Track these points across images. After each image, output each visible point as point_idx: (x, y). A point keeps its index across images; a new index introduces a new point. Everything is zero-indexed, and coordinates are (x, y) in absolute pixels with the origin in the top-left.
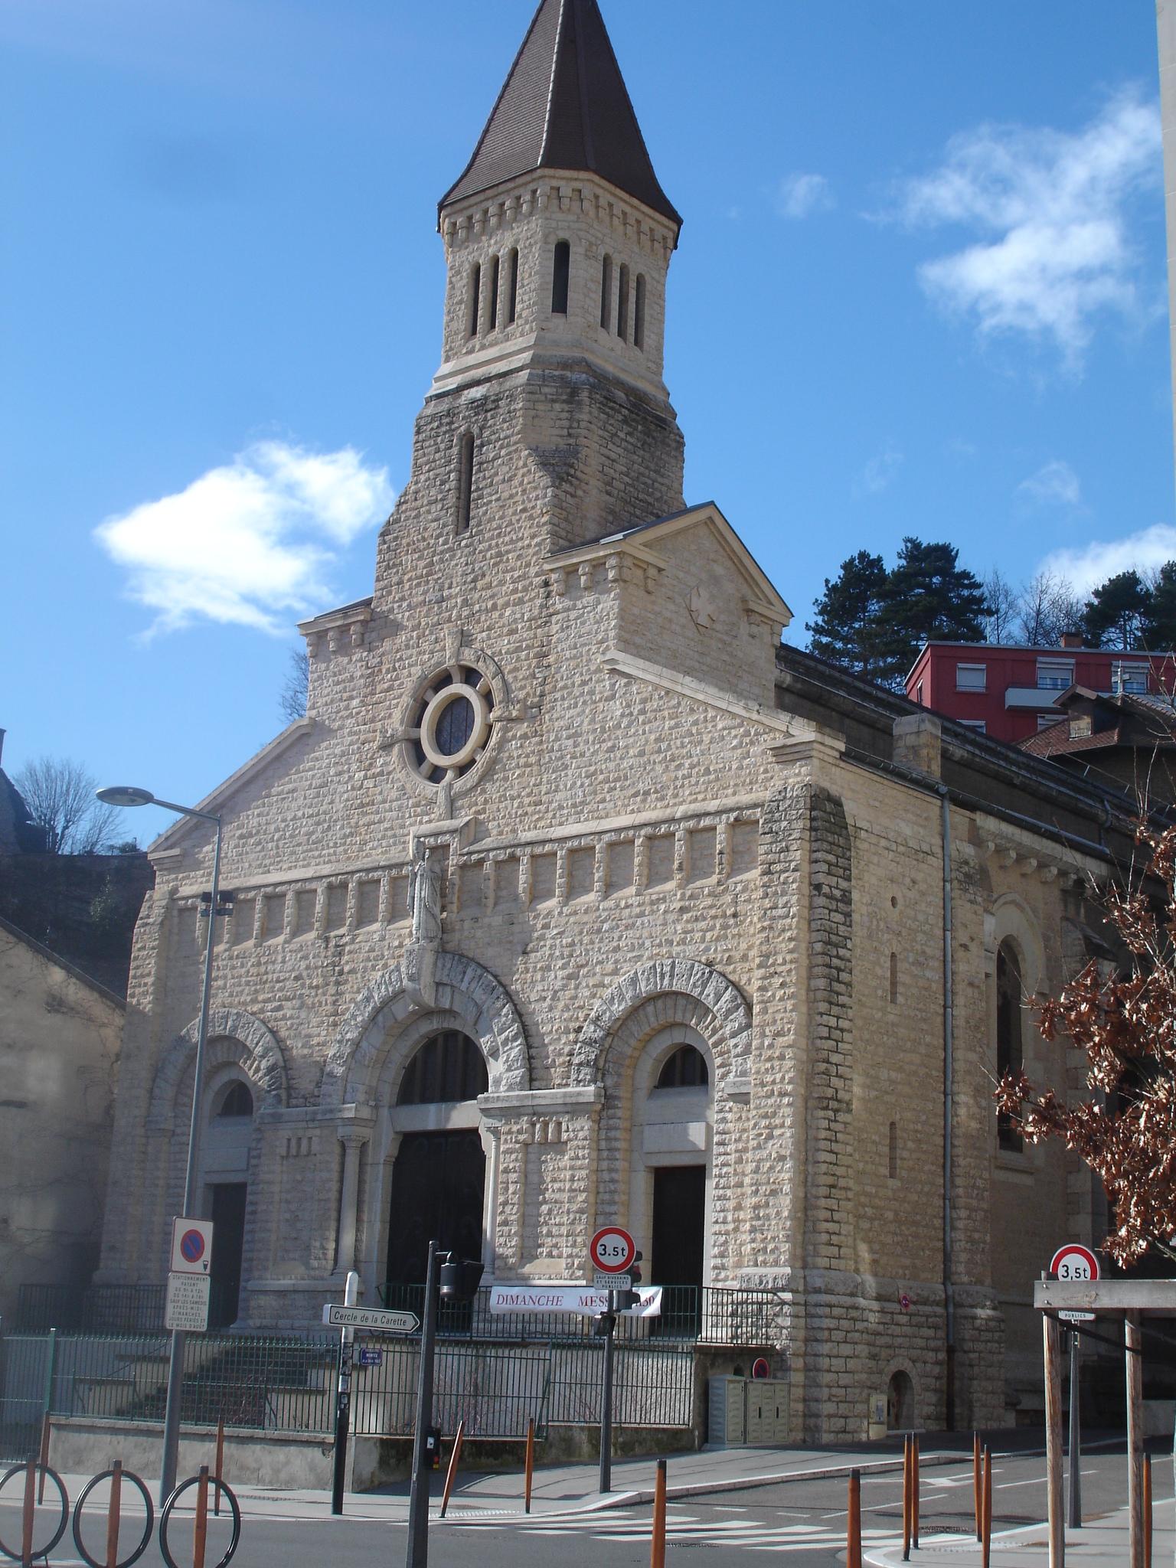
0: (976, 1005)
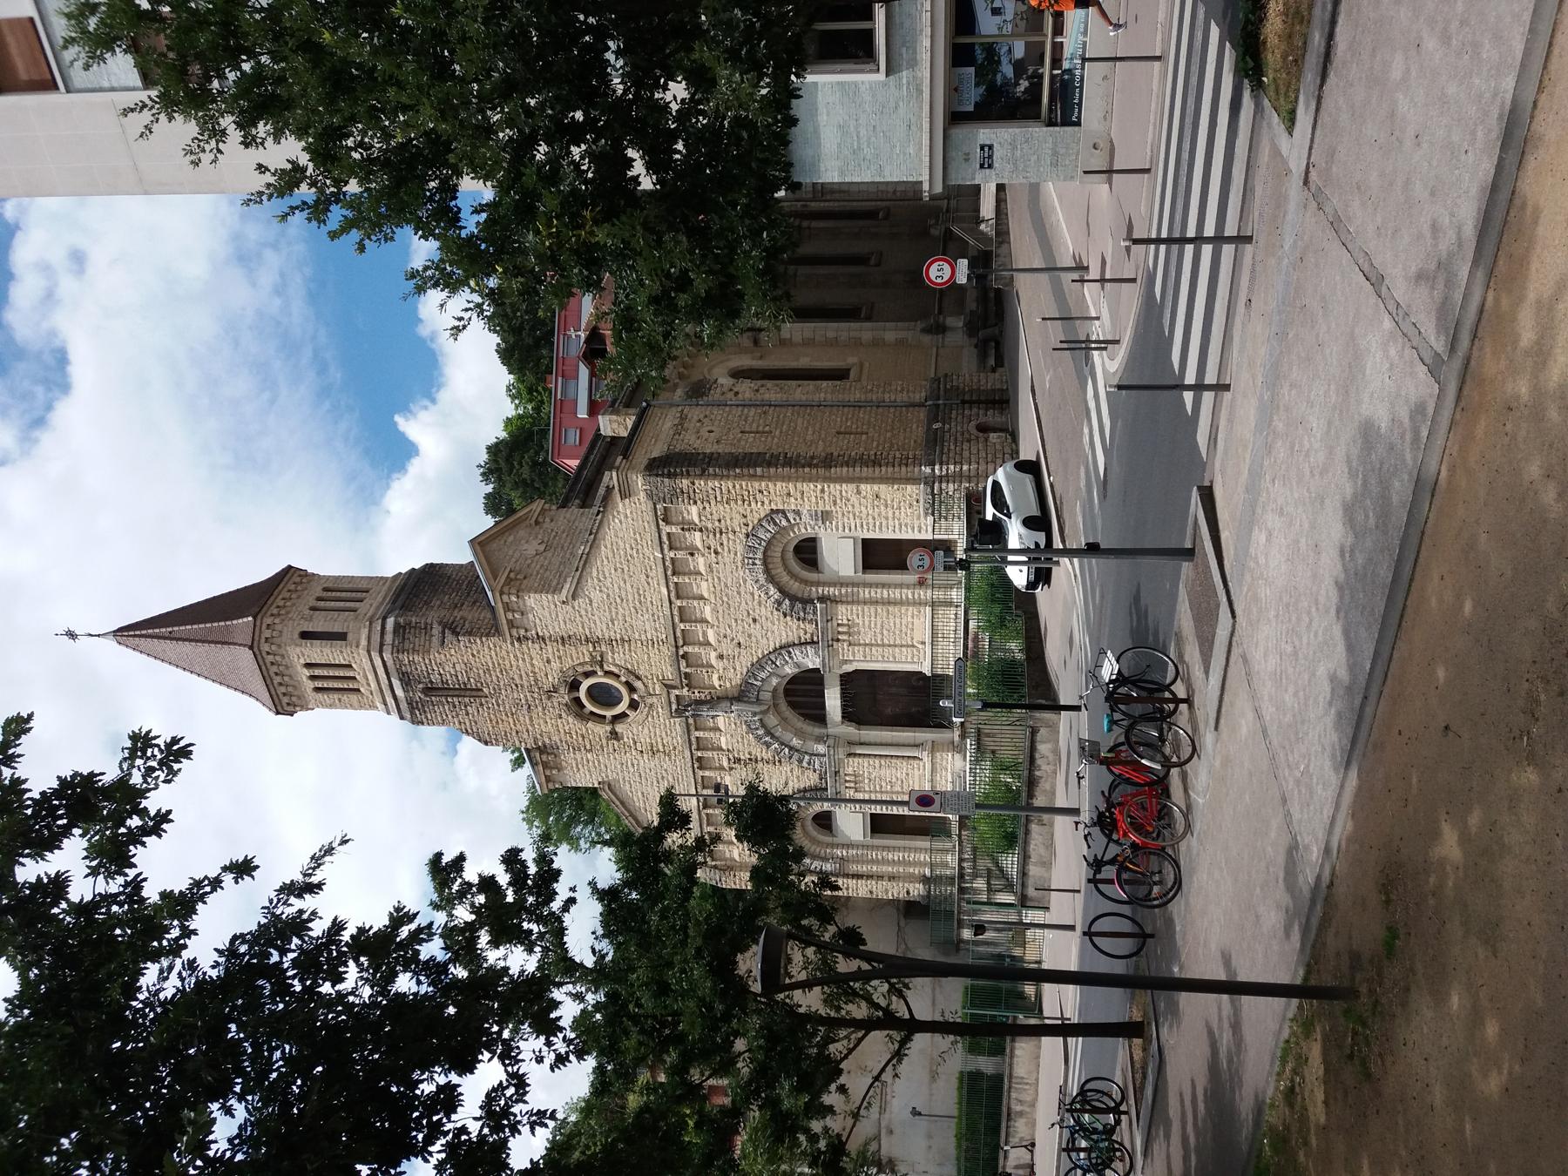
0: (772, 391)
